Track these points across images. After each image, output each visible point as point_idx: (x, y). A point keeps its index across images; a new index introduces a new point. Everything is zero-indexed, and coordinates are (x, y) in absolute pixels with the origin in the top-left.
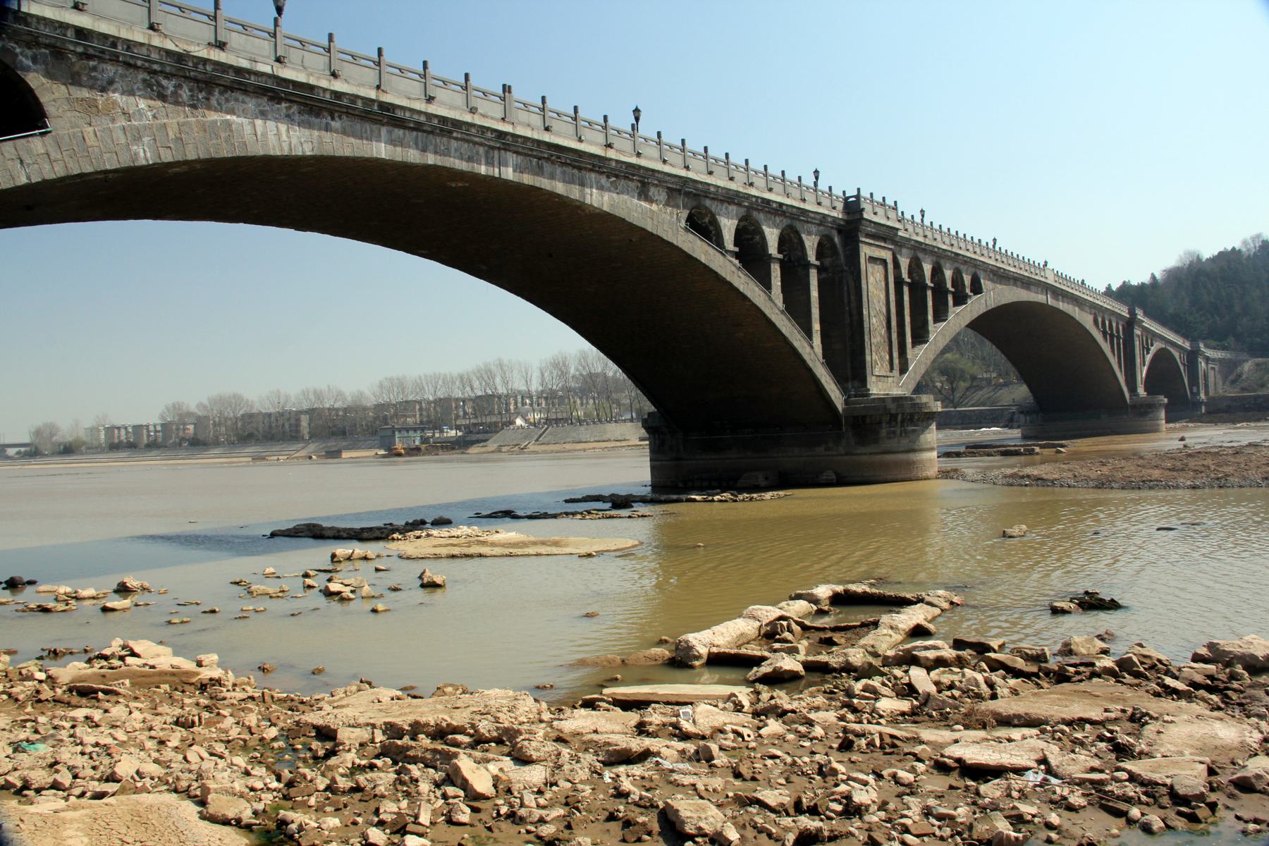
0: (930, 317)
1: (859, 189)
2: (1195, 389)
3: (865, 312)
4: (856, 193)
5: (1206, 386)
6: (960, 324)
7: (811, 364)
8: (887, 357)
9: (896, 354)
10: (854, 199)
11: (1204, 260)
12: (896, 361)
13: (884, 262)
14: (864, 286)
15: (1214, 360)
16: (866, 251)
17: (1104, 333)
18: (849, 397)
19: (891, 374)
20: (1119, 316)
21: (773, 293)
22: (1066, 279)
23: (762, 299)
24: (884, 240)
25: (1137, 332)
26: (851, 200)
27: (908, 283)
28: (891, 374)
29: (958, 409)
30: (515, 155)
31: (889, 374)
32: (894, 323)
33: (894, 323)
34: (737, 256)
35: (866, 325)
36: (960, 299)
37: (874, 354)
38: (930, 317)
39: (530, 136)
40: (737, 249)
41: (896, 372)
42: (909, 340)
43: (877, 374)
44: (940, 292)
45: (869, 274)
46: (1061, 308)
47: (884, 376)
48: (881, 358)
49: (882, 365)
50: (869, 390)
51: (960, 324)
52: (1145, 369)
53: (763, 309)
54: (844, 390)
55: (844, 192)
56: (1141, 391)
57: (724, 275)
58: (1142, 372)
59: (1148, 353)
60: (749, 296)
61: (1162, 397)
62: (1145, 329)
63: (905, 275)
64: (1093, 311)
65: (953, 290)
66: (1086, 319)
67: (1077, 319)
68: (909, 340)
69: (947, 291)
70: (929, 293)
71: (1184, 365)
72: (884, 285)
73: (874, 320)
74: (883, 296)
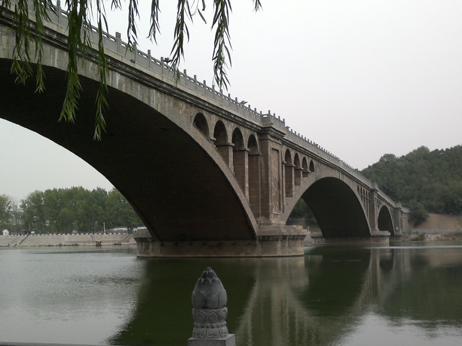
0: (293, 183)
1: (269, 111)
2: (397, 229)
4: (268, 113)
8: (278, 204)
10: (266, 116)
11: (399, 158)
13: (278, 151)
14: (269, 164)
15: (405, 213)
16: (271, 145)
17: (362, 196)
21: (229, 165)
22: (348, 167)
23: (225, 168)
24: (278, 139)
25: (375, 196)
26: (265, 116)
30: (119, 74)
34: (215, 142)
35: (270, 186)
36: (306, 174)
38: (293, 183)
39: (129, 65)
40: (215, 139)
42: (285, 195)
43: (274, 213)
46: (153, 105)
48: (276, 204)
50: (271, 221)
52: (378, 216)
55: (261, 112)
56: (377, 228)
59: (378, 208)
62: (379, 196)
63: (284, 160)
64: (357, 184)
66: (353, 187)
70: (293, 170)
71: (392, 215)
73: (273, 183)
74: (277, 171)
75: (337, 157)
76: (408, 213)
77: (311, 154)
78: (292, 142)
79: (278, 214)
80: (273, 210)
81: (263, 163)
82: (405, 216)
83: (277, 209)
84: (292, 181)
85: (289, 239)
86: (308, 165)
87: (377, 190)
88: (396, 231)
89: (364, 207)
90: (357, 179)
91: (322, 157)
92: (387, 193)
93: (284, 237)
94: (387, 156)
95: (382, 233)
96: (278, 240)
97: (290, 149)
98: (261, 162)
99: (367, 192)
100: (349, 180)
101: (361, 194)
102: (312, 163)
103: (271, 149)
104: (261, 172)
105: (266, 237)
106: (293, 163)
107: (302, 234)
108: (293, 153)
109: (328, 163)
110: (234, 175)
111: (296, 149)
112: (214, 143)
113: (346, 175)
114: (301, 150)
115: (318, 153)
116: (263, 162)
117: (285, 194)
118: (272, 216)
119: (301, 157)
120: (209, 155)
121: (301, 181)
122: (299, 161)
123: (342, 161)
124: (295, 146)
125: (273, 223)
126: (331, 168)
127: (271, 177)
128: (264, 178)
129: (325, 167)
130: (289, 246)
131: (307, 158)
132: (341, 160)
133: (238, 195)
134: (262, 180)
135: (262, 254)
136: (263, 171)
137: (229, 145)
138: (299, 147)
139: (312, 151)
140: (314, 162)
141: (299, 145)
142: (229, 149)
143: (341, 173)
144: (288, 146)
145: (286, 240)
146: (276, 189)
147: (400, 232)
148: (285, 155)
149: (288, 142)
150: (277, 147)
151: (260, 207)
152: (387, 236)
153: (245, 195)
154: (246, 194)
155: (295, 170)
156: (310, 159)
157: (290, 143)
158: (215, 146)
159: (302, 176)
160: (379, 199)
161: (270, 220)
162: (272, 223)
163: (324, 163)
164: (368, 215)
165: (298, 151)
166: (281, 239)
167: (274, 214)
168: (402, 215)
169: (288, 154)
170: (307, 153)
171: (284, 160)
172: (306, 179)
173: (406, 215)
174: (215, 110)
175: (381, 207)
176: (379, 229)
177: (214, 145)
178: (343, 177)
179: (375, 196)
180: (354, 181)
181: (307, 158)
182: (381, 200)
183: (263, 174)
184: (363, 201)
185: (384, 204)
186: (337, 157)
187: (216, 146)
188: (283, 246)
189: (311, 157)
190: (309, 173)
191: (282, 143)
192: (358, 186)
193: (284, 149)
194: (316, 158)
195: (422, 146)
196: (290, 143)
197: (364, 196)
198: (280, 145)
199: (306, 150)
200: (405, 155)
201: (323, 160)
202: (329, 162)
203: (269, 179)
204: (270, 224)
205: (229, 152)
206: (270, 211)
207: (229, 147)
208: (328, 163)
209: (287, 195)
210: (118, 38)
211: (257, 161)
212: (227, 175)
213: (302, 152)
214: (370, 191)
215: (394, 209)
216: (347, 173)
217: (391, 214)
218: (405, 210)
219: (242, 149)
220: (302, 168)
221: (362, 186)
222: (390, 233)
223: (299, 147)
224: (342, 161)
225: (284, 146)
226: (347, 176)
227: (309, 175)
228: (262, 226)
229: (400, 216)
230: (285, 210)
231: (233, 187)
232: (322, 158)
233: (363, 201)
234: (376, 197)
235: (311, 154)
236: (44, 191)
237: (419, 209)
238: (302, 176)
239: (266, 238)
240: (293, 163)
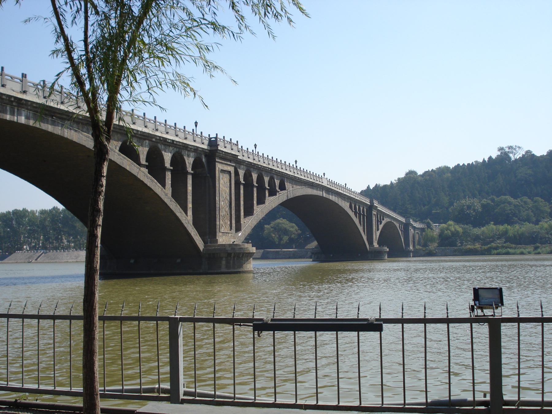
0: (255, 202)
1: (217, 134)
4: (215, 136)
8: (229, 223)
10: (214, 139)
14: (217, 185)
15: (418, 229)
16: (219, 166)
17: (355, 213)
26: (212, 139)
28: (230, 232)
31: (229, 232)
35: (217, 206)
36: (273, 193)
38: (255, 202)
40: (147, 164)
42: (242, 213)
47: (227, 233)
49: (225, 227)
55: (209, 135)
59: (381, 224)
66: (345, 205)
68: (242, 213)
71: (402, 231)
74: (228, 191)
103: (220, 170)
133: (177, 215)
148: (243, 175)
164: (364, 231)
167: (222, 232)
174: (143, 137)
179: (373, 212)
184: (362, 226)
185: (386, 220)
200: (434, 169)
203: (217, 199)
206: (217, 230)
210: (24, 78)
233: (362, 226)
234: (375, 213)
236: (11, 211)
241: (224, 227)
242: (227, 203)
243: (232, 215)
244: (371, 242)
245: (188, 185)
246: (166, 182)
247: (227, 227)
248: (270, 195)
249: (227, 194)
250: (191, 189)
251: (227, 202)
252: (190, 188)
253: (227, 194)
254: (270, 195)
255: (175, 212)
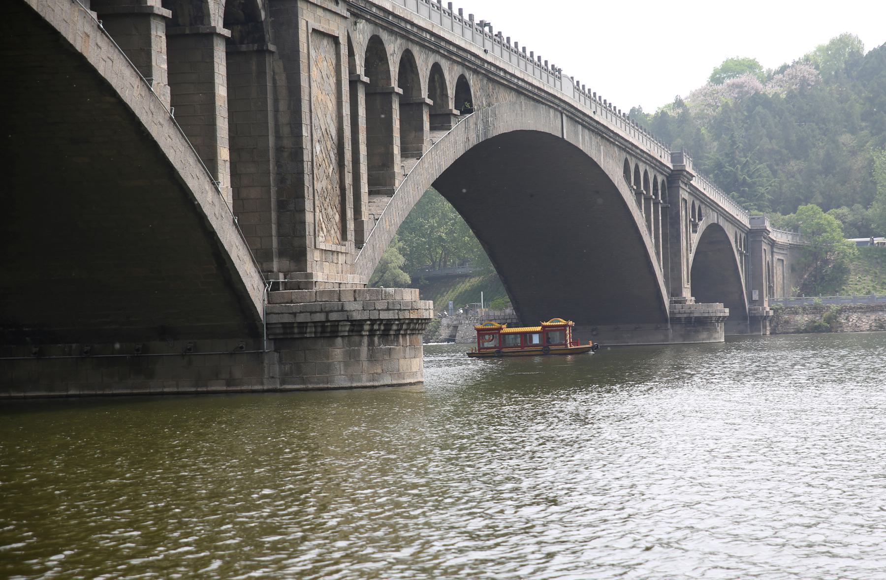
0: (397, 150)
2: (755, 297)
3: (305, 133)
5: (771, 288)
6: (440, 166)
7: (215, 223)
8: (337, 217)
9: (350, 213)
12: (351, 225)
13: (335, 40)
14: (304, 84)
15: (782, 247)
17: (638, 194)
18: (275, 286)
19: (343, 249)
20: (657, 165)
21: (154, 82)
25: (684, 194)
27: (227, 39)
28: (343, 249)
29: (429, 344)
31: (339, 248)
32: (348, 155)
33: (348, 155)
35: (307, 157)
36: (441, 121)
37: (317, 210)
38: (397, 150)
41: (350, 245)
42: (364, 188)
43: (322, 247)
44: (411, 107)
45: (312, 62)
47: (333, 252)
49: (328, 231)
51: (440, 166)
52: (691, 257)
53: (137, 112)
54: (265, 274)
56: (687, 293)
57: (70, 39)
58: (687, 259)
59: (695, 231)
60: (114, 85)
61: (719, 306)
62: (695, 192)
63: (360, 70)
65: (400, 91)
66: (614, 170)
67: (602, 167)
68: (364, 188)
69: (391, 92)
70: (396, 106)
71: (741, 254)
72: (333, 86)
73: (318, 148)
74: (331, 106)
75: (500, 33)
76: (792, 247)
77: (461, 53)
78: (391, 10)
79: (338, 252)
80: (320, 239)
81: (282, 81)
82: (781, 257)
83: (336, 233)
84: (391, 143)
85: (372, 333)
86: (451, 92)
87: (688, 172)
88: (751, 301)
89: (645, 228)
90: (623, 138)
91: (497, 64)
92: (728, 186)
93: (356, 326)
94: (731, 68)
95: (702, 309)
96: (337, 337)
97: (385, 36)
98: (277, 77)
99: (655, 178)
100: (596, 140)
101: (635, 187)
102: (463, 86)
103: (310, 31)
104: (276, 111)
105: (293, 327)
106: (394, 84)
107: (416, 317)
108: (394, 49)
109: (520, 83)
110: (171, 118)
111: (405, 35)
112: (89, 5)
113: (583, 126)
114: (425, 40)
115: (486, 51)
116: (284, 76)
117: (367, 185)
118: (317, 255)
119: (424, 64)
120: (71, 45)
121: (425, 144)
122: (417, 74)
123: (572, 78)
124: (403, 24)
125: (320, 279)
126: (532, 103)
127: (309, 127)
128: (286, 130)
129: (511, 97)
130: (372, 358)
131: (445, 65)
132: (566, 77)
134: (278, 137)
135: (283, 382)
136: (283, 106)
137: (150, 12)
138: (415, 30)
139: (463, 45)
140: (473, 81)
141: (416, 22)
142: (153, 26)
143: (567, 116)
144: (376, 24)
145: (363, 336)
146: (331, 170)
147: (766, 304)
149: (374, 10)
150: (336, 27)
151: (274, 227)
152: (719, 319)
153: (217, 189)
154: (222, 183)
155: (401, 105)
156: (458, 70)
157: (381, 14)
158: (94, 15)
159: (427, 125)
160: (697, 203)
161: (309, 271)
162: (314, 280)
163: (505, 83)
164: (658, 254)
165: (413, 41)
166: (346, 334)
168: (772, 252)
169: (375, 49)
170: (445, 49)
171: (363, 73)
172: (440, 135)
173: (785, 252)
175: (702, 226)
176: (693, 298)
177: (89, 11)
178: (576, 133)
179: (681, 192)
180: (614, 144)
181: (445, 65)
182: (703, 207)
183: (284, 119)
184: (643, 208)
185: (712, 218)
186: (500, 33)
187: (99, 17)
188: (352, 357)
189: (458, 63)
190: (455, 115)
191: (349, 14)
192: (626, 160)
193: (362, 34)
194: (478, 66)
195: (850, 36)
196: (381, 14)
197: (645, 192)
198: (343, 20)
199: (443, 39)
201: (502, 74)
202: (523, 80)
203: (305, 133)
204: (308, 283)
205: (153, 37)
206: (309, 241)
207: (152, 19)
208: (520, 83)
209: (374, 189)
211: (262, 73)
212: (144, 119)
213: (423, 45)
214: (665, 175)
215: (747, 234)
216: (587, 119)
217: (738, 250)
218: (781, 237)
219: (202, 29)
220: (429, 101)
221: (640, 160)
222: (727, 310)
223: (415, 30)
224: (572, 78)
225: (362, 25)
226: (589, 129)
227: (452, 124)
228: (282, 290)
229: (766, 257)
230: (367, 238)
231: (171, 158)
232: (501, 69)
233: (643, 208)
235: (461, 53)
237: (826, 232)
238: (427, 125)
239: (296, 330)
240: (397, 83)
241: (325, 230)
242: (329, 148)
243: (347, 192)
244: (675, 292)
245: (216, 81)
246: (154, 63)
247: (333, 232)
248: (433, 128)
249: (328, 116)
250: (226, 95)
251: (329, 144)
252: (221, 91)
253: (328, 116)
254: (433, 128)
255: (182, 173)
